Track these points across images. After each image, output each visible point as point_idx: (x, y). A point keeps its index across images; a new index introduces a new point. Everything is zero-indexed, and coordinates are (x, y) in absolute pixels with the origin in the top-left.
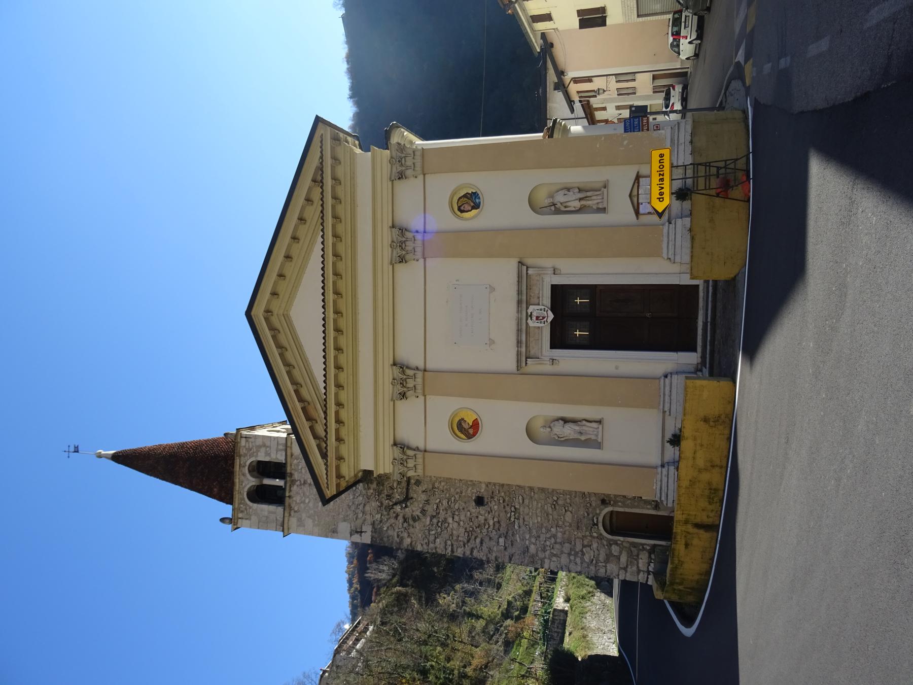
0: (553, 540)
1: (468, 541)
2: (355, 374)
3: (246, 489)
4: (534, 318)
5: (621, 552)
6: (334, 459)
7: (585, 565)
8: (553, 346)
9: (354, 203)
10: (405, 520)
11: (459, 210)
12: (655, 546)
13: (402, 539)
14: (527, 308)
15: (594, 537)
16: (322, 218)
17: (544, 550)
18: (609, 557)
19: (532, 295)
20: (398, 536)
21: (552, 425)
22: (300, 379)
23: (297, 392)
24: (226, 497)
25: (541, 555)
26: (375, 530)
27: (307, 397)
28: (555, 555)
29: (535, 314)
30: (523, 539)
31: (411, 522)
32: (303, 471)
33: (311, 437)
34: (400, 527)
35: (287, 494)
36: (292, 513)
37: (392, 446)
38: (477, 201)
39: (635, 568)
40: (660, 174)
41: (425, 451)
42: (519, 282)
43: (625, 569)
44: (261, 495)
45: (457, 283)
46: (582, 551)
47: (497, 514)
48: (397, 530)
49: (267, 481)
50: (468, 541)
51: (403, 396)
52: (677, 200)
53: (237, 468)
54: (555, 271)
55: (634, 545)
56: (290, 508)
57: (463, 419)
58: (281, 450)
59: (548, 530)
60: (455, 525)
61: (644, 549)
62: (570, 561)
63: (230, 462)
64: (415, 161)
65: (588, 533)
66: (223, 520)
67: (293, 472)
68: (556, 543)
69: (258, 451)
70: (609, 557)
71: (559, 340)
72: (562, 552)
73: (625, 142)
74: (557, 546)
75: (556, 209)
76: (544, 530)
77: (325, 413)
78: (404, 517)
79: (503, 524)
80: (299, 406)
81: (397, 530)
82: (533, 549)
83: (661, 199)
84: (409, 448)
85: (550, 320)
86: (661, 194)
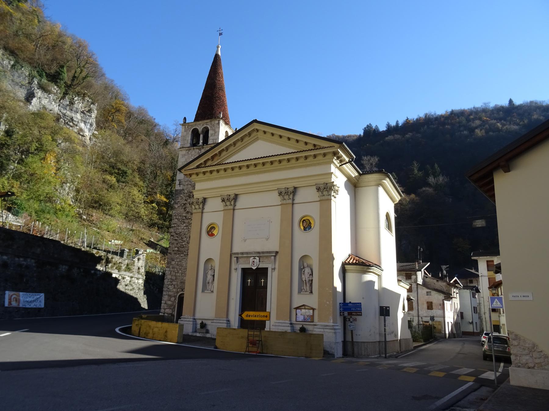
0: (176, 271)
1: (176, 234)
2: (232, 176)
3: (197, 127)
4: (253, 260)
5: (172, 301)
6: (196, 172)
7: (167, 286)
8: (243, 270)
9: (306, 166)
10: (184, 204)
11: (304, 220)
12: (174, 316)
13: (177, 204)
14: (258, 257)
15: (177, 290)
16: (301, 151)
17: (173, 268)
18: (170, 296)
19: (264, 259)
20: (178, 202)
21: (212, 270)
22: (229, 150)
23: (223, 150)
24: (197, 119)
25: (171, 266)
26: (181, 190)
27: (222, 155)
28: (171, 273)
29: (255, 260)
30: (177, 259)
31: (184, 207)
32: (192, 157)
33: (204, 160)
34: (182, 202)
35: (195, 148)
36: (187, 151)
37: (294, 187)
38: (307, 229)
39: (166, 307)
40: (258, 316)
41: (293, 204)
42: (267, 252)
43: (165, 303)
44: (195, 134)
45: (271, 222)
46: (172, 284)
47: (187, 246)
48: (181, 201)
49: (201, 136)
50: (176, 234)
51: (223, 200)
52: (300, 328)
53: (206, 121)
54: (274, 269)
55: (174, 307)
56: (189, 150)
57: (215, 229)
58: (213, 141)
59: (180, 269)
60: (182, 227)
61: (173, 311)
62: (169, 279)
63: (209, 117)
64: (325, 196)
65: (179, 287)
66: (185, 119)
67: (204, 148)
68: (176, 273)
69: (213, 130)
70: (170, 296)
71: (246, 272)
72: (172, 276)
73: (328, 303)
74: (174, 274)
75: (301, 270)
76: (180, 267)
77: (215, 165)
78: (186, 203)
79: (183, 249)
80: (217, 152)
81: (181, 201)
82: (173, 263)
83: (247, 316)
84: (294, 195)
85: (253, 267)
86: (249, 316)
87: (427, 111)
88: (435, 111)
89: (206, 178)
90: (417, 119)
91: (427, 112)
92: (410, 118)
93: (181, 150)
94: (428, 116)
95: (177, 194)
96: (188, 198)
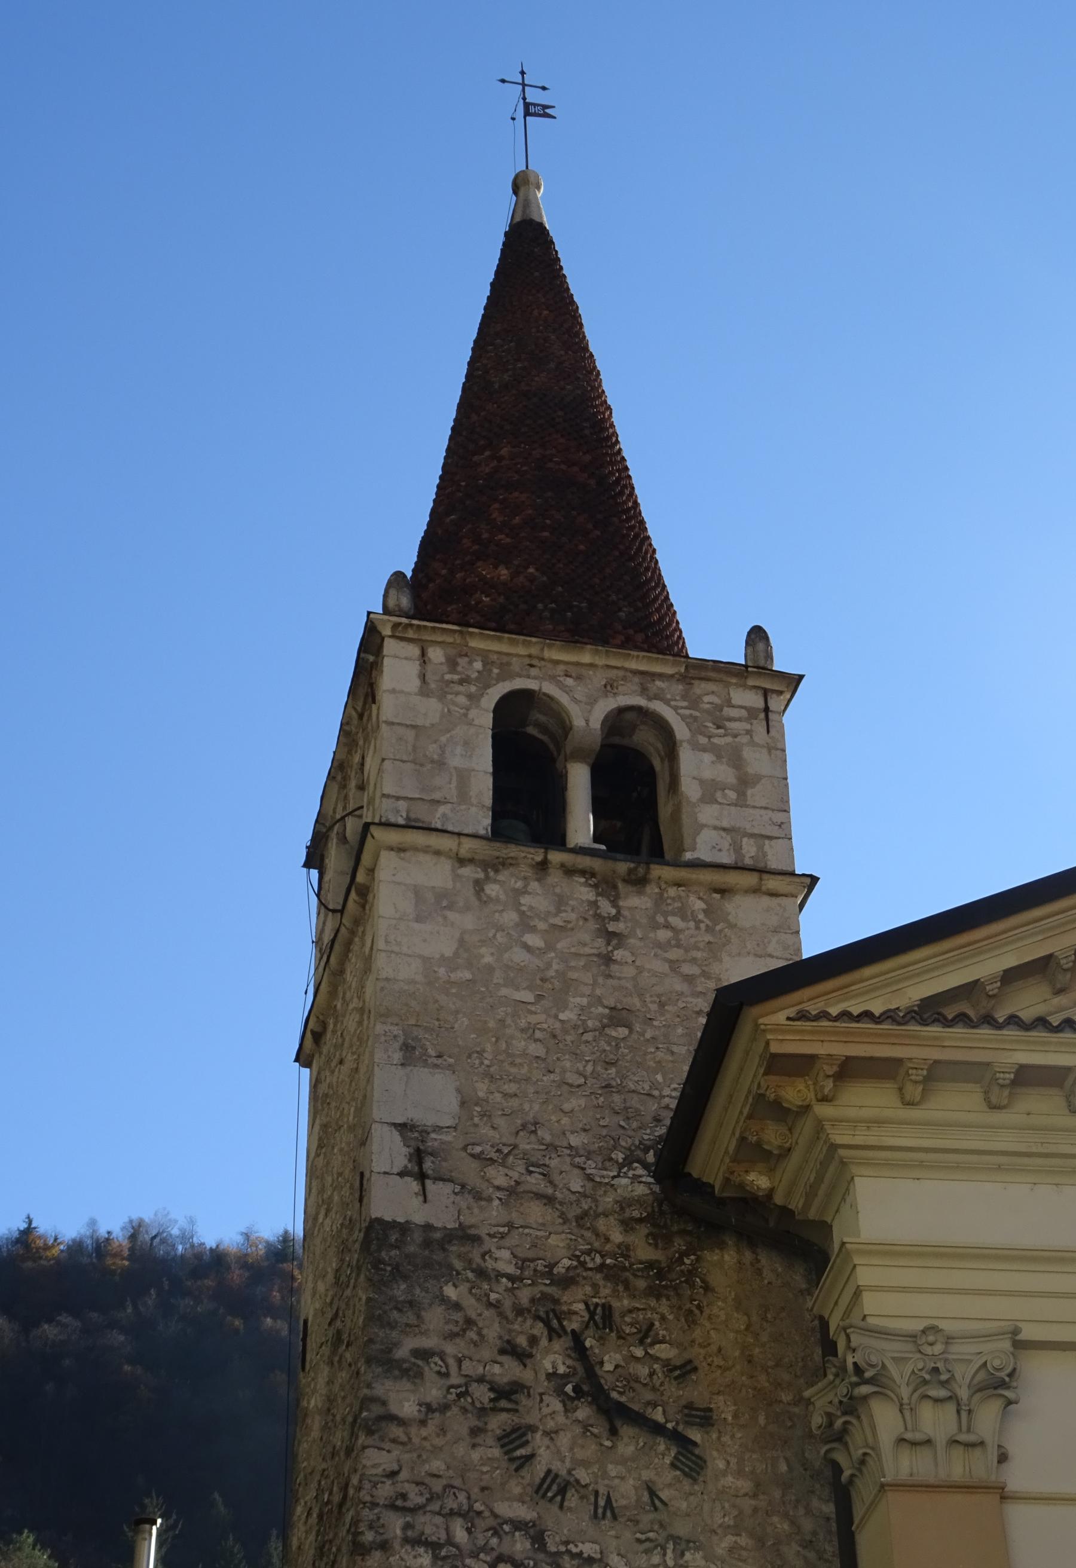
31: (497, 1423)
48: (450, 1349)
67: (652, 889)
81: (450, 1349)
87: (146, 1212)
88: (192, 1221)
89: (1006, 1142)
90: (76, 1247)
91: (147, 1216)
92: (44, 1226)
93: (401, 849)
94: (147, 1238)
95: (398, 1274)
96: (539, 1329)
